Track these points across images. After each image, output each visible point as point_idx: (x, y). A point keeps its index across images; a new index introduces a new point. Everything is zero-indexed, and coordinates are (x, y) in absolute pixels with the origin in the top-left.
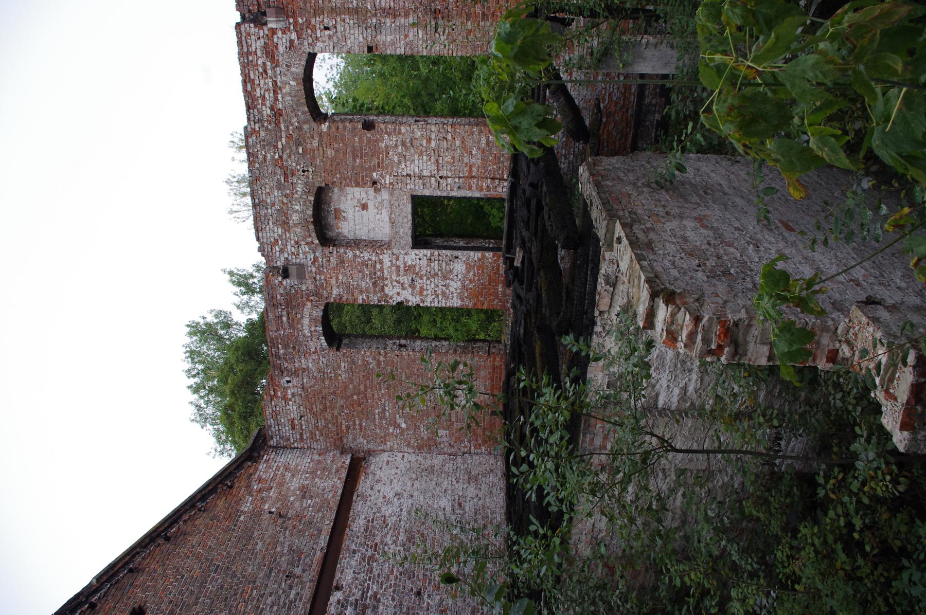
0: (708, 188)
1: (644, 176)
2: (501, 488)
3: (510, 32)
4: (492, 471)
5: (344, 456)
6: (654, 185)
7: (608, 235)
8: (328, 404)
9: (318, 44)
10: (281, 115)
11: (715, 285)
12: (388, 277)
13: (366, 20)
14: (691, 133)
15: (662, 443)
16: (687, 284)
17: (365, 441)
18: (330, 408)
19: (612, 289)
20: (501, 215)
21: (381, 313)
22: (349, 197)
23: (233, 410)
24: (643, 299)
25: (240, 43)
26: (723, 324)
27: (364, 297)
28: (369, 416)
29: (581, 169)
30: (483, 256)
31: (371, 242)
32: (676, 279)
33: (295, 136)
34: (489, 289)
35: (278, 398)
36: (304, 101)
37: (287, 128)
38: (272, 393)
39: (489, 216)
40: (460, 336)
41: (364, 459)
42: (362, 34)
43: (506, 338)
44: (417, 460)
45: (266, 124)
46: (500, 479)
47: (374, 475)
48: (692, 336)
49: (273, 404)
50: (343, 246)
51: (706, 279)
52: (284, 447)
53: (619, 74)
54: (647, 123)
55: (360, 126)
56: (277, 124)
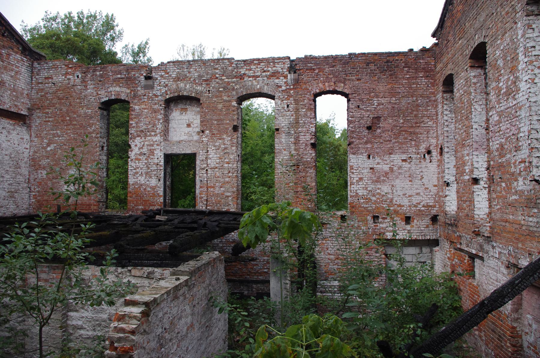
0: (209, 328)
1: (215, 290)
2: (5, 213)
3: (305, 218)
4: (18, 206)
5: (27, 110)
6: (210, 296)
7: (180, 272)
8: (63, 101)
9: (280, 101)
10: (241, 79)
11: (154, 340)
12: (147, 139)
13: (293, 127)
14: (241, 314)
15: (46, 319)
16: (154, 323)
17: (37, 124)
18: (61, 103)
19: (145, 276)
20: (186, 206)
21: (122, 134)
22: (194, 117)
23: (56, 40)
24: (144, 298)
25: (279, 58)
26: (131, 349)
27: (133, 125)
28: (55, 127)
29: (217, 253)
30: (161, 196)
31: (168, 129)
32: (157, 316)
33: (229, 87)
34: (140, 201)
35: (67, 69)
36: (249, 92)
37: (234, 82)
38: (70, 66)
39: (184, 199)
40: (109, 183)
41: (25, 123)
42: (285, 126)
43: (109, 212)
44: (24, 157)
45: (235, 70)
46: (12, 212)
47: (14, 130)
48: (122, 330)
49: (63, 66)
50: (165, 112)
51: (158, 334)
52: (32, 72)
53: (269, 269)
54: (242, 287)
55: (235, 124)
56: (236, 77)
